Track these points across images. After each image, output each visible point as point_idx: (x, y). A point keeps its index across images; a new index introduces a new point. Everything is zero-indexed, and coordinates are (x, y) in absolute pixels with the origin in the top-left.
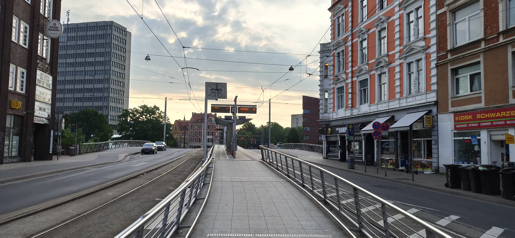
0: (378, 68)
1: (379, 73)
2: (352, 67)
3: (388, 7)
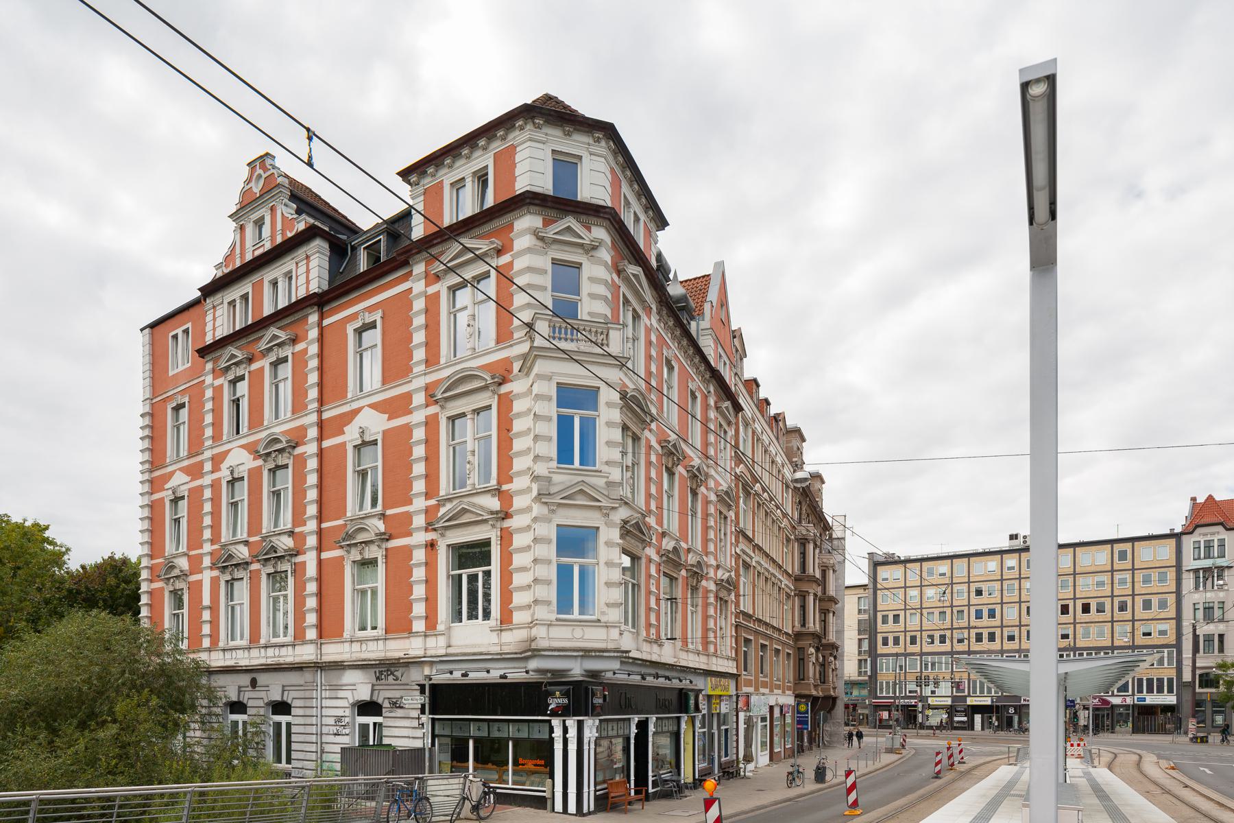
0: (226, 567)
1: (229, 578)
2: (320, 518)
3: (295, 419)
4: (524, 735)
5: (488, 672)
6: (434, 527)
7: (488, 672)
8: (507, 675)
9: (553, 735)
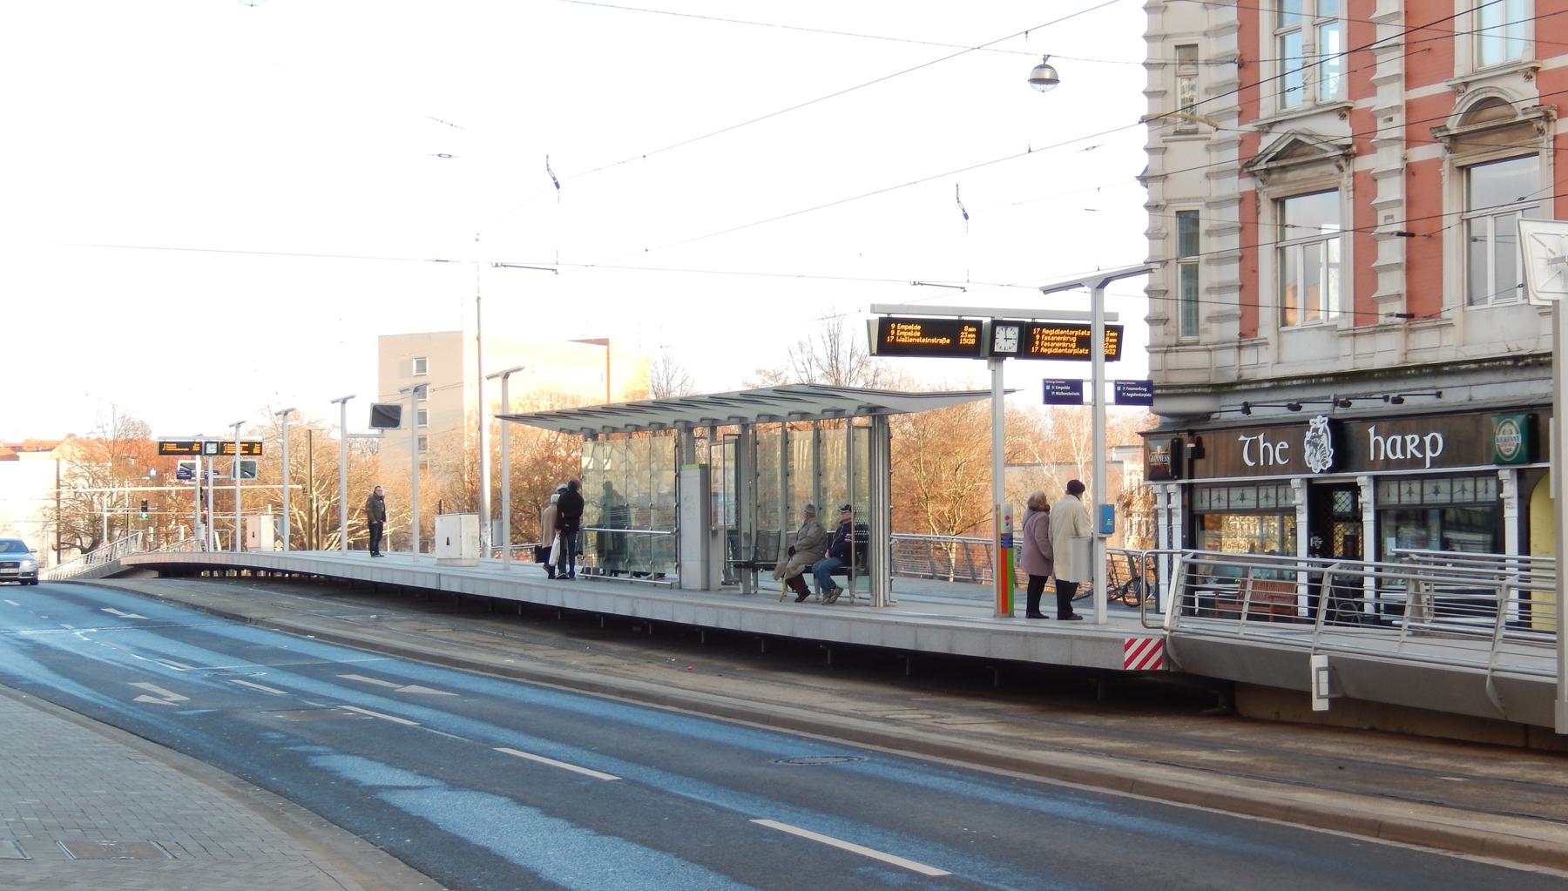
4: (1443, 498)
5: (1439, 395)
6: (1251, 169)
7: (1439, 395)
8: (1403, 397)
9: (1502, 495)
